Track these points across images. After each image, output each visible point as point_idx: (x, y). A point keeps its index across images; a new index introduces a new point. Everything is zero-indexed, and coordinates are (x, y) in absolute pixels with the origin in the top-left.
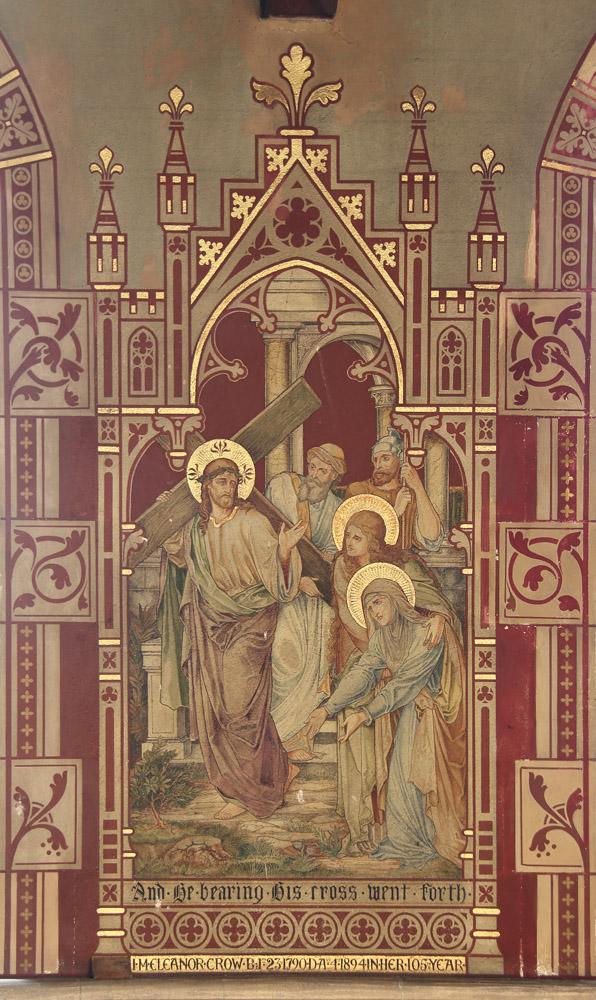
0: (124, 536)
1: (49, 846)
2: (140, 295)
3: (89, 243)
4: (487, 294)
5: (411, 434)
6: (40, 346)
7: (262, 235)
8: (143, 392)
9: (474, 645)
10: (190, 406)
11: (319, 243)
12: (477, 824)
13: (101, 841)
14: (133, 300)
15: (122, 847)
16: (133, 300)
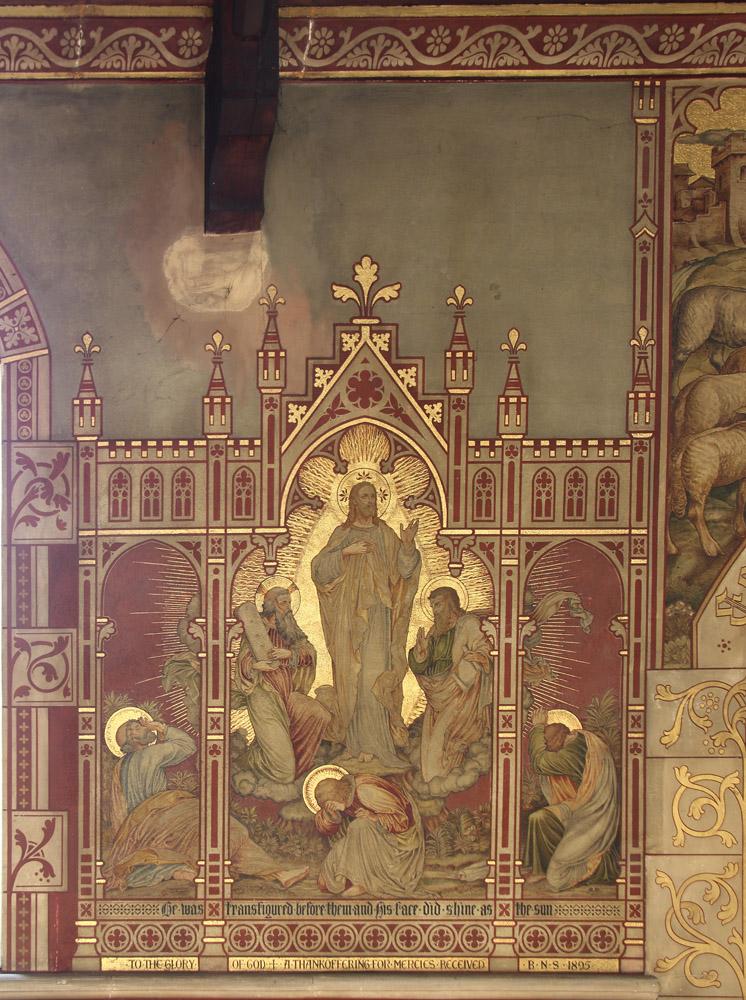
0: (520, 626)
1: (41, 875)
2: (242, 442)
3: (628, 399)
4: (511, 443)
5: (266, 547)
6: (39, 485)
7: (337, 400)
8: (483, 518)
9: (207, 712)
10: (279, 527)
11: (382, 405)
12: (208, 858)
13: (80, 871)
14: (237, 446)
15: (223, 875)
16: (237, 446)
